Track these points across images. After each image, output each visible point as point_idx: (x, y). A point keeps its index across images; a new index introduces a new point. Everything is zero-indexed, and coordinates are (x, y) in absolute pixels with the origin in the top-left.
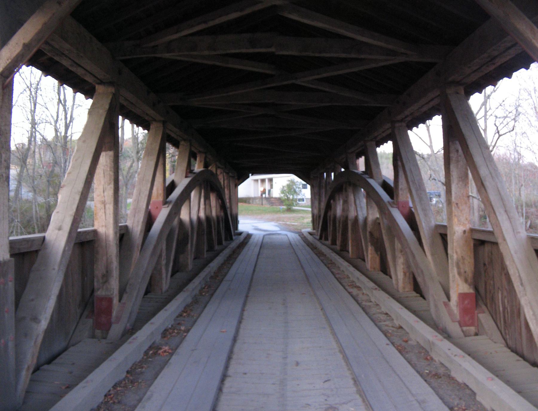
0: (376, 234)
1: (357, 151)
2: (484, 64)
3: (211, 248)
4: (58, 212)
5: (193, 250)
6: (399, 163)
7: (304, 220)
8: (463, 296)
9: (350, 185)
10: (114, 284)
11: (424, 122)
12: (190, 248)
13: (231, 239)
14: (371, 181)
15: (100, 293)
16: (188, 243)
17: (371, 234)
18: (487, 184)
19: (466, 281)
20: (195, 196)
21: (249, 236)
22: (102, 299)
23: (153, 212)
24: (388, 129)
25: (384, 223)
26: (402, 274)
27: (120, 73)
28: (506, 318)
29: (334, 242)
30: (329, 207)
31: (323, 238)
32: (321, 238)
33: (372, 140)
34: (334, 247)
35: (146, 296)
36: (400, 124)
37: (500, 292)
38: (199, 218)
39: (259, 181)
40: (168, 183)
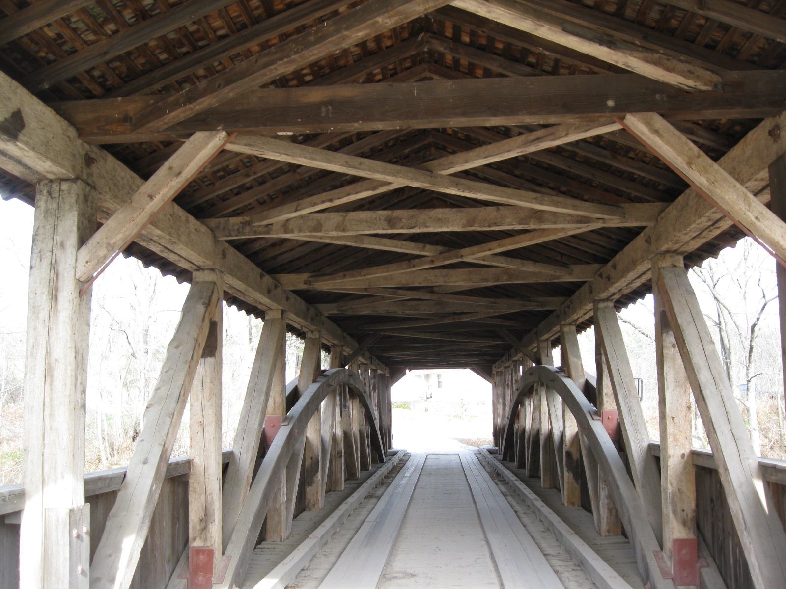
0: (575, 456)
1: (553, 338)
2: (706, 229)
3: (350, 475)
4: (142, 441)
5: (325, 481)
6: (603, 359)
7: (483, 434)
8: (680, 544)
9: (542, 385)
10: (215, 529)
11: (692, 268)
12: (320, 477)
13: (382, 461)
14: (568, 382)
15: (197, 544)
16: (317, 471)
17: (569, 454)
18: (707, 393)
19: (684, 523)
20: (327, 405)
21: (407, 455)
22: (198, 551)
23: (269, 433)
24: (591, 310)
25: (584, 440)
26: (606, 510)
27: (224, 255)
28: (738, 574)
29: (522, 465)
30: (515, 415)
31: (508, 459)
32: (504, 459)
33: (570, 324)
34: (521, 471)
35: (259, 546)
36: (605, 304)
37: (730, 538)
38: (334, 437)
39: (423, 377)
40: (288, 391)
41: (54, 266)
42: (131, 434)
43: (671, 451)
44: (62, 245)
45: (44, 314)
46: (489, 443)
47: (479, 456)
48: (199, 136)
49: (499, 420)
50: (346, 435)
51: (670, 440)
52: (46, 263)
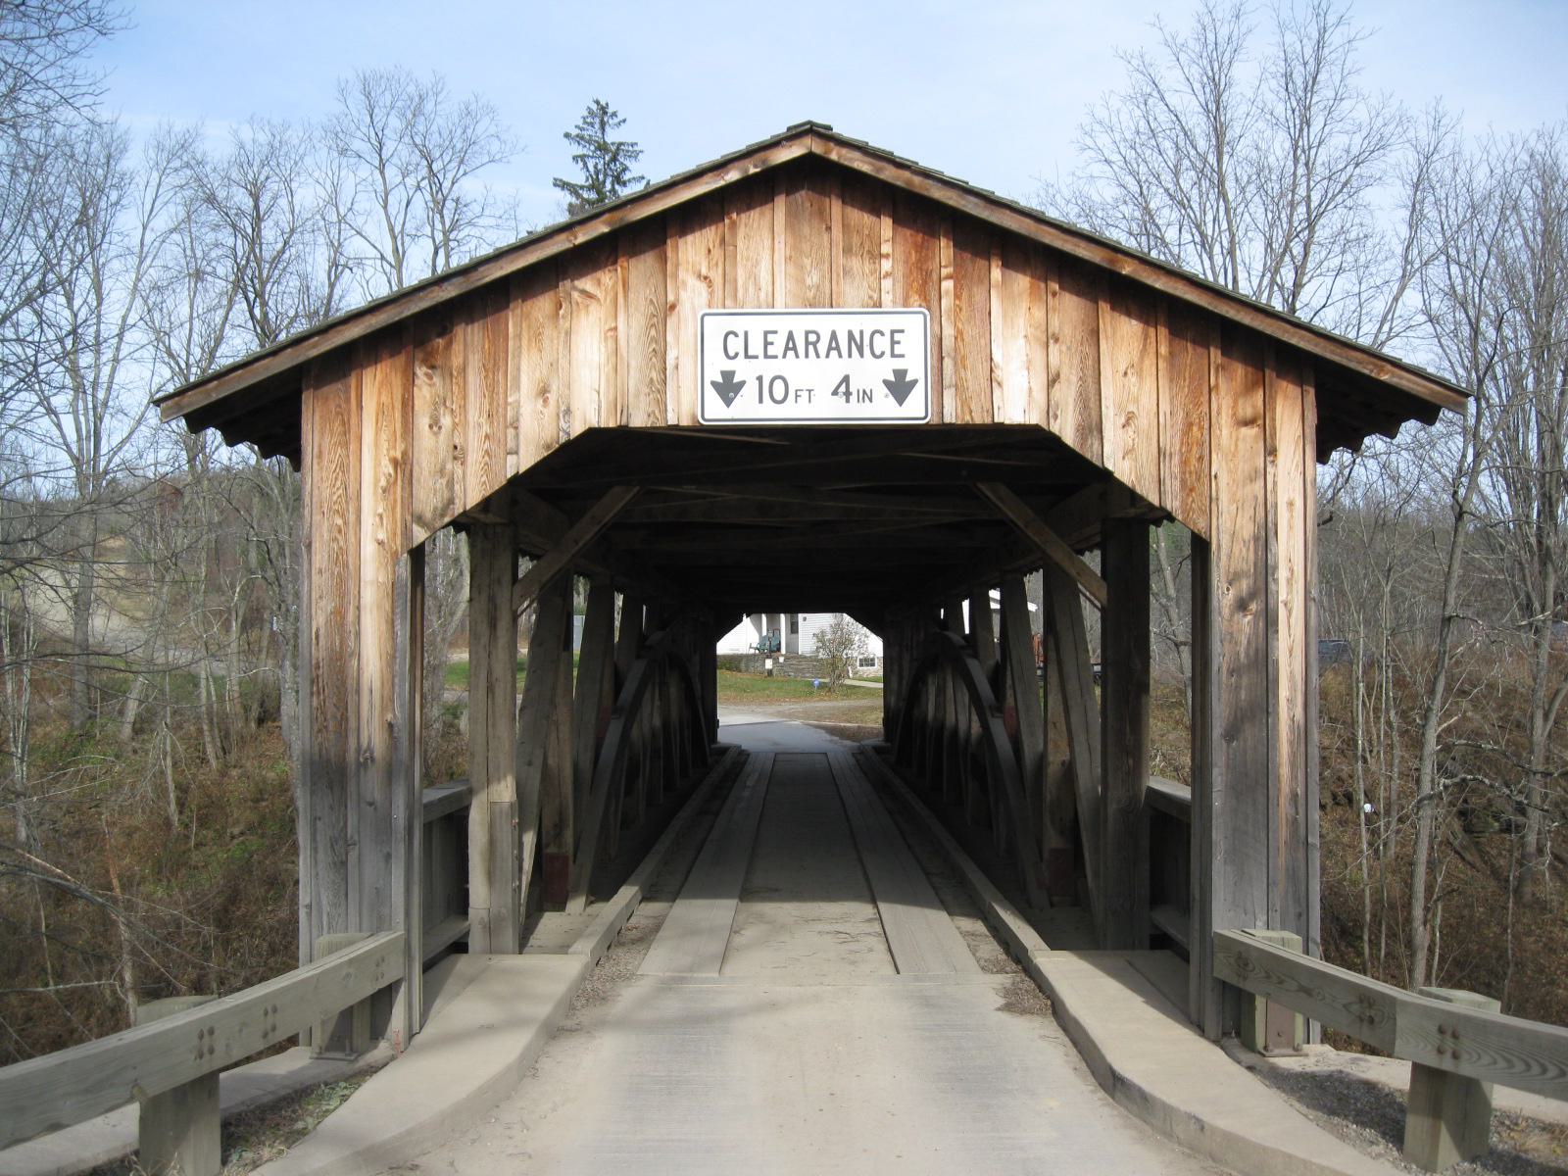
41: (492, 599)
42: (254, 714)
43: (1051, 758)
44: (499, 582)
45: (484, 640)
46: (877, 736)
47: (859, 757)
48: (617, 489)
49: (893, 700)
50: (666, 724)
51: (1050, 746)
52: (484, 596)
